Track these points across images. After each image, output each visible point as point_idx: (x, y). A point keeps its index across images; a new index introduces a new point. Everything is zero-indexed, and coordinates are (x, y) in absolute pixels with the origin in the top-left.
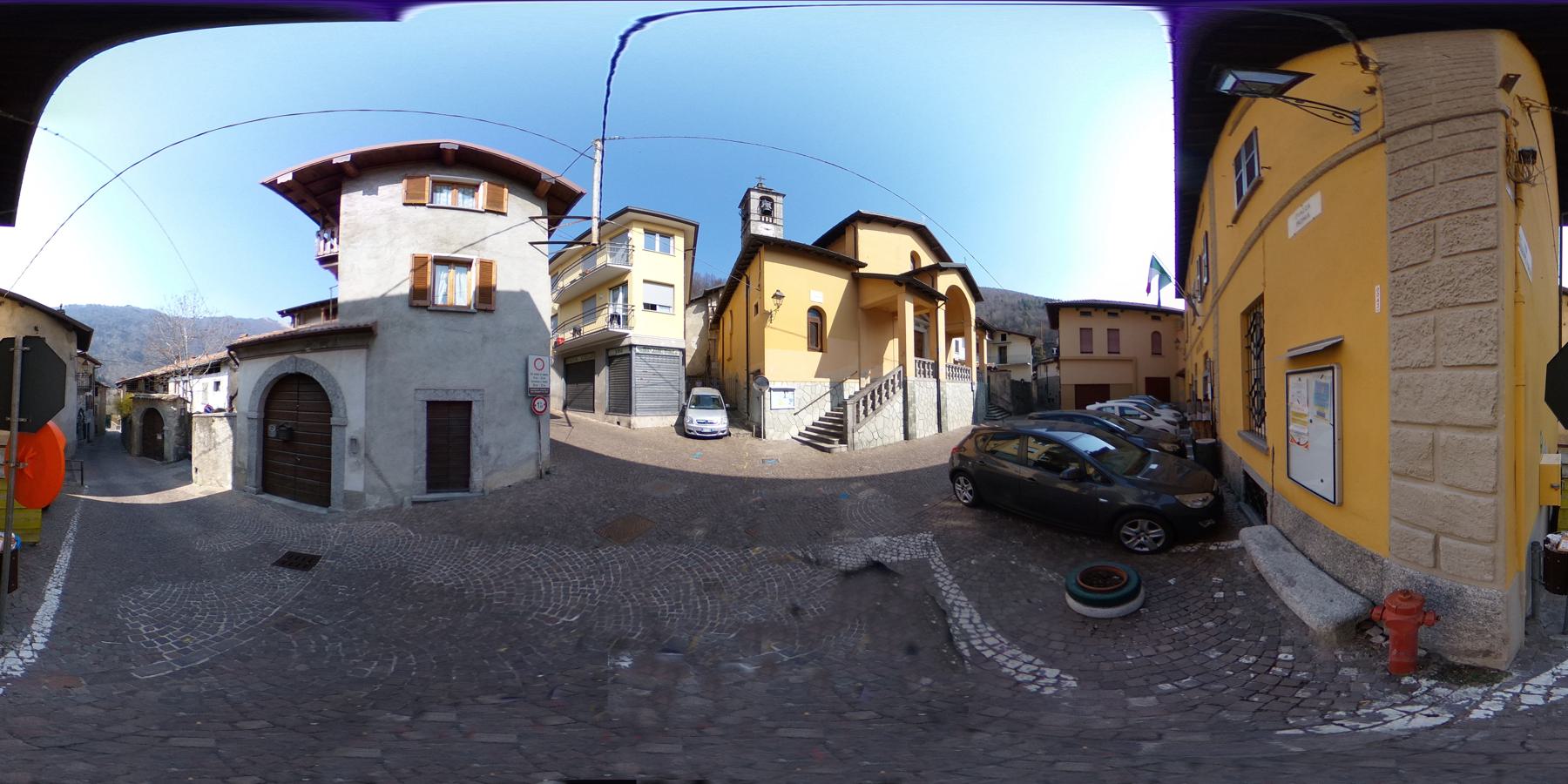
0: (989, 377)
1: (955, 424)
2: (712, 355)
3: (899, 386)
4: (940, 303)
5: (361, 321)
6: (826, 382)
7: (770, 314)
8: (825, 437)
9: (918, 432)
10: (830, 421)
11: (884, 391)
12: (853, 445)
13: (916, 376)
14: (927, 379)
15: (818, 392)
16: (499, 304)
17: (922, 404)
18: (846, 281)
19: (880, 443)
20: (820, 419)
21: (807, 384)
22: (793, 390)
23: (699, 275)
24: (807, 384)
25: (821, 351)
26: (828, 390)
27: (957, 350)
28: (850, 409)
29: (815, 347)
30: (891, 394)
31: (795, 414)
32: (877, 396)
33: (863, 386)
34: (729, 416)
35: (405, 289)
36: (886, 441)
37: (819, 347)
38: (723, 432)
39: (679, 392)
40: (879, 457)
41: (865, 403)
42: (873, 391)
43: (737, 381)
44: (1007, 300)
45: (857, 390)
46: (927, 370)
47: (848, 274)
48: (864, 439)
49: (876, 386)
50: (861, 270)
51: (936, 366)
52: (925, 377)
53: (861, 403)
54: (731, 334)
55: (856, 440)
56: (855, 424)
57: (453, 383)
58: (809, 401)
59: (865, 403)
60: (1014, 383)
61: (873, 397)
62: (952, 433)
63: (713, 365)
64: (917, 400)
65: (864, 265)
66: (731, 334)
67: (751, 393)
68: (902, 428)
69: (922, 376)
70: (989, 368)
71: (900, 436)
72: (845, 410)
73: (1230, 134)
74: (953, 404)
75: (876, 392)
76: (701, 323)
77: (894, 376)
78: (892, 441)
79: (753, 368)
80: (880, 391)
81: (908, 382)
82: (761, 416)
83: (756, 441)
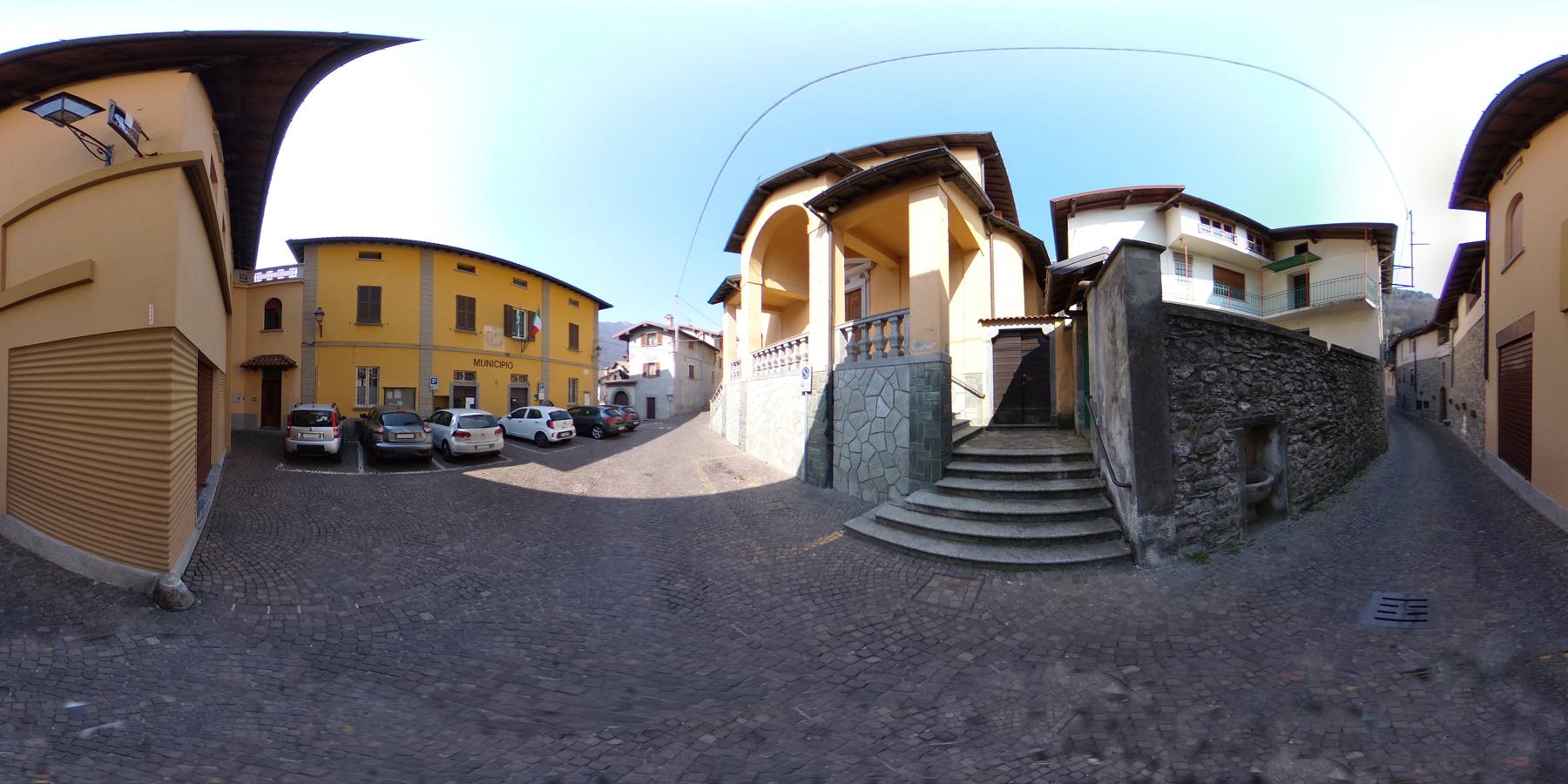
5: (633, 380)
16: (661, 374)
35: (641, 373)
57: (652, 394)
73: (515, 281)
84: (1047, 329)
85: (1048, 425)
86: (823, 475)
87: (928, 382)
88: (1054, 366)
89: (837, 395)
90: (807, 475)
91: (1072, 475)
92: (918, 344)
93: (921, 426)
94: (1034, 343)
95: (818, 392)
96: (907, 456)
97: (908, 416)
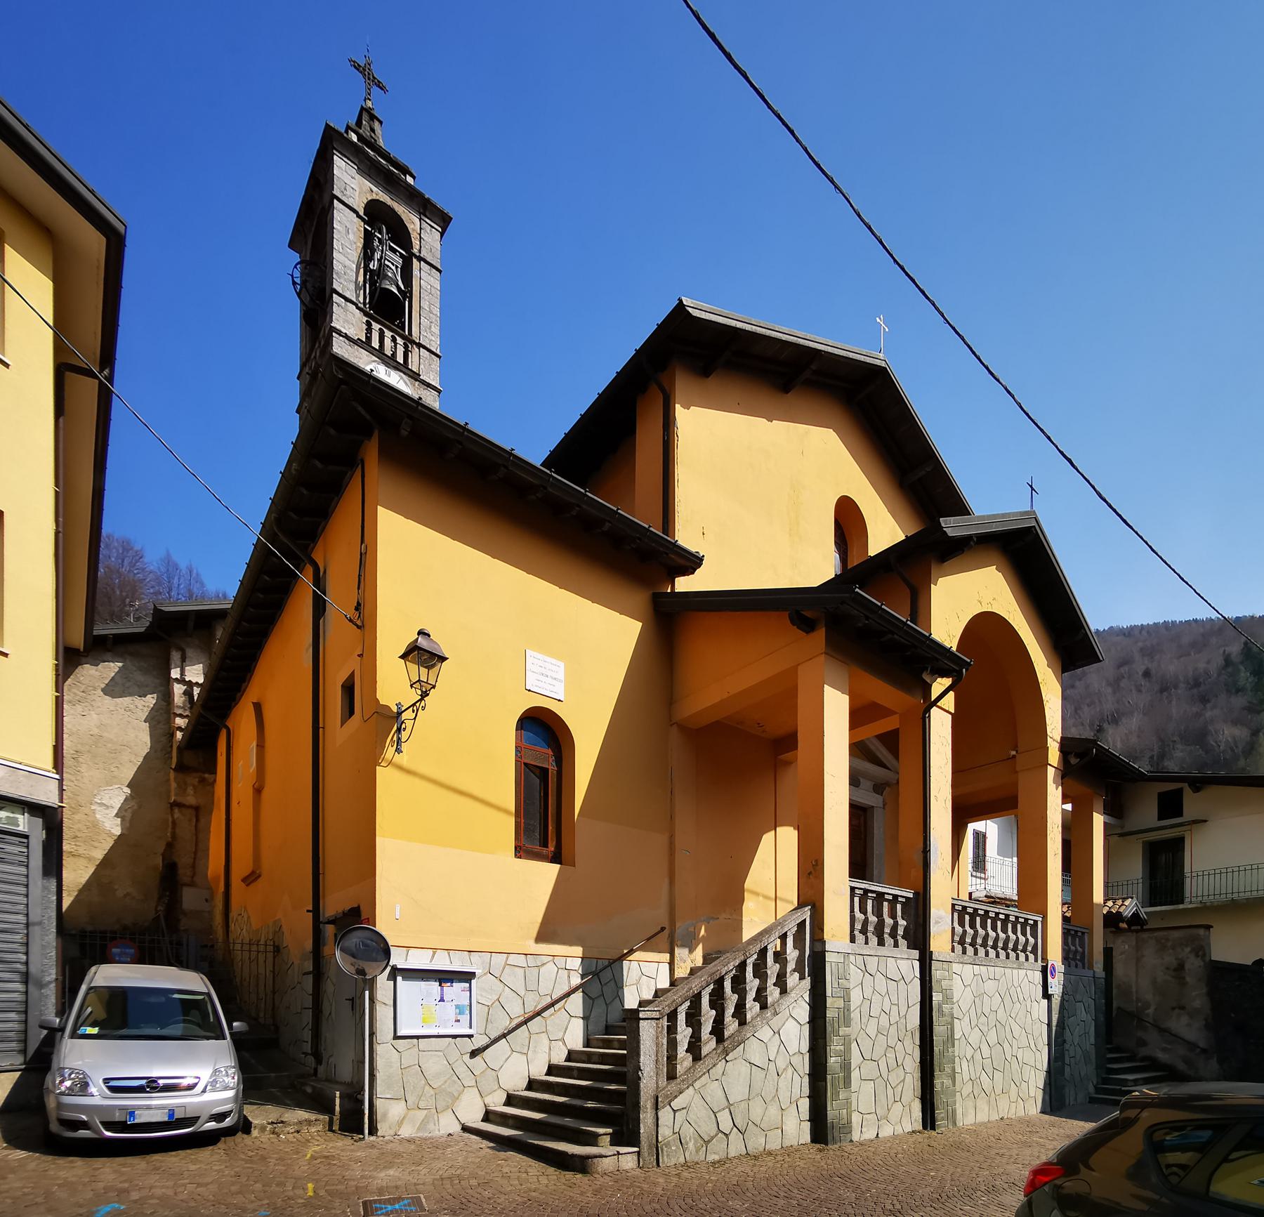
0: (1108, 953)
1: (982, 1104)
2: (183, 860)
3: (799, 968)
4: (939, 685)
6: (572, 957)
7: (391, 720)
8: (568, 1121)
9: (856, 1118)
10: (582, 1074)
11: (752, 984)
12: (657, 1148)
13: (853, 940)
14: (888, 949)
15: (545, 987)
17: (872, 1031)
18: (638, 626)
19: (736, 1147)
20: (552, 1069)
21: (513, 959)
22: (467, 977)
23: (139, 556)
24: (513, 959)
25: (556, 858)
26: (576, 980)
27: (979, 863)
28: (649, 1034)
29: (538, 848)
30: (773, 993)
31: (474, 1054)
32: (731, 1000)
33: (681, 972)
34: (244, 1066)
36: (757, 1142)
37: (552, 848)
38: (220, 1117)
39: (26, 978)
40: (737, 1190)
41: (694, 1019)
42: (720, 982)
43: (277, 950)
44: (1171, 666)
45: (664, 983)
46: (889, 921)
47: (640, 598)
48: (688, 1132)
49: (728, 967)
50: (684, 584)
51: (919, 909)
52: (881, 943)
53: (682, 1018)
54: (258, 791)
55: (665, 1132)
56: (663, 1081)
58: (517, 1012)
59: (694, 1019)
60: (1221, 973)
61: (717, 1000)
62: (974, 1131)
63: (190, 898)
64: (855, 1015)
65: (691, 563)
66: (258, 791)
67: (329, 987)
68: (805, 1104)
69: (874, 940)
70: (1112, 920)
71: (797, 1129)
72: (633, 1045)
74: (975, 1037)
75: (728, 985)
76: (140, 740)
77: (783, 937)
78: (774, 1145)
79: (334, 905)
80: (739, 983)
81: (829, 957)
82: (362, 1060)
83: (342, 1144)
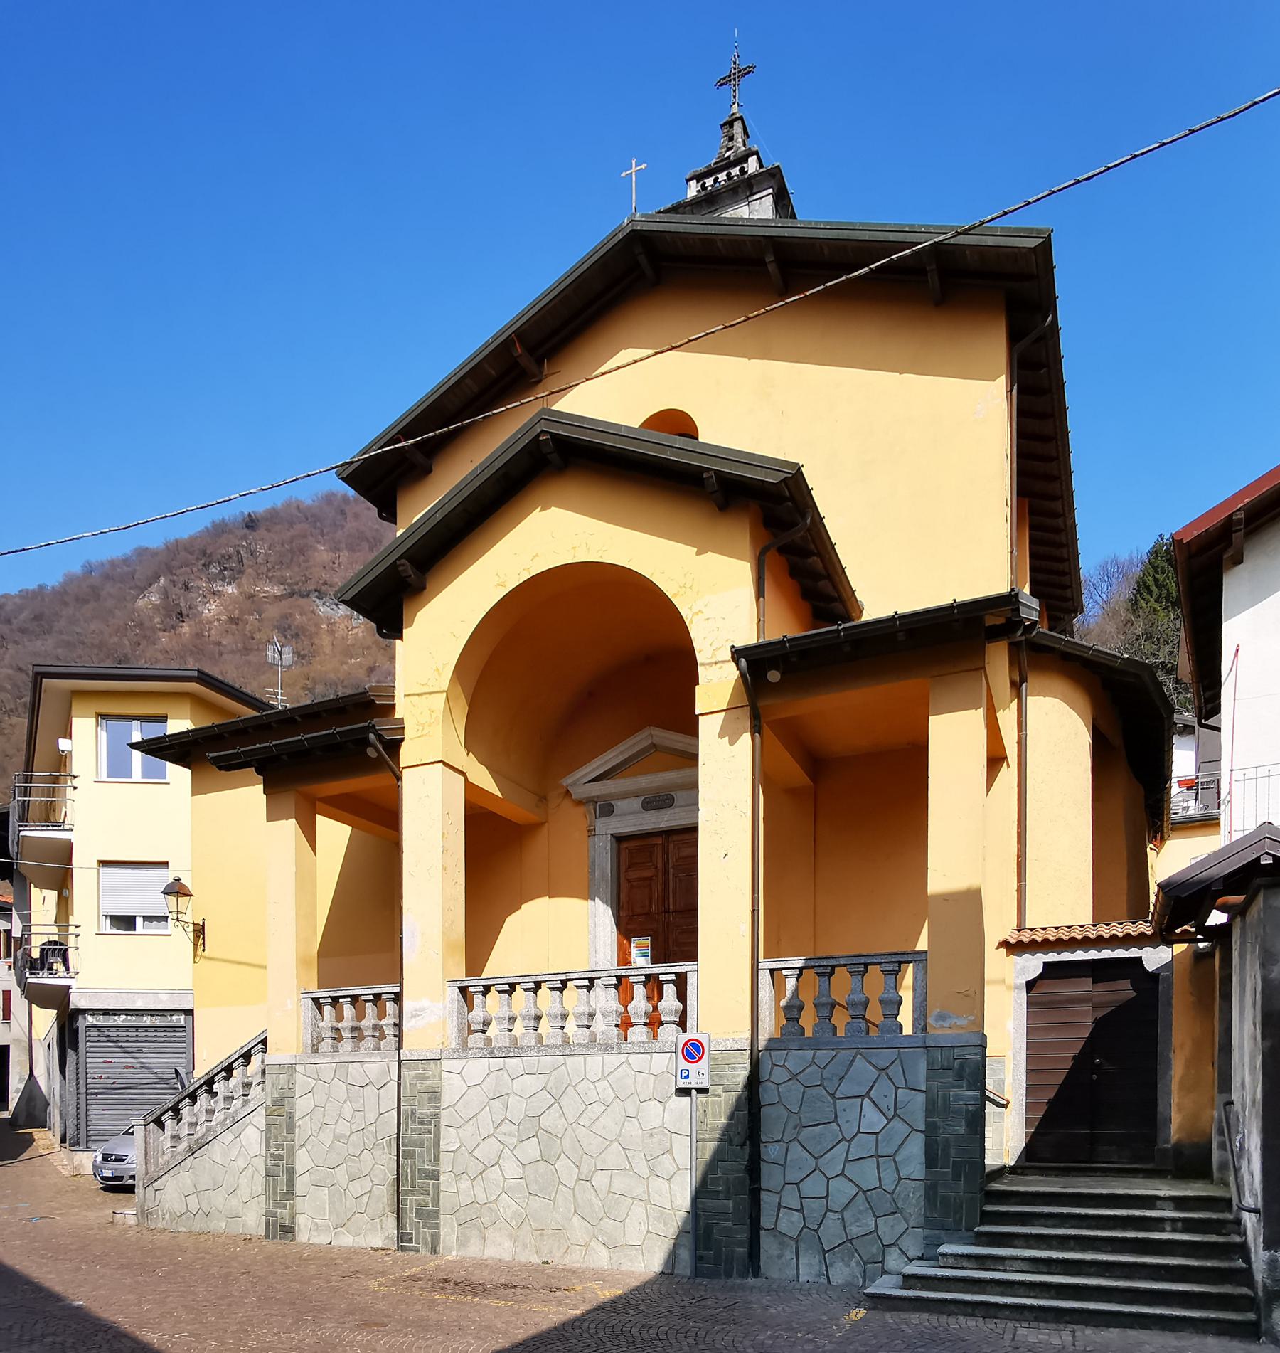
84: (1154, 958)
85: (1149, 1166)
86: (742, 1251)
87: (960, 1077)
88: (1168, 1041)
89: (768, 1094)
90: (698, 1259)
91: (1189, 1226)
92: (942, 1017)
93: (947, 1146)
94: (1123, 990)
95: (726, 1090)
96: (921, 1192)
97: (923, 1128)
